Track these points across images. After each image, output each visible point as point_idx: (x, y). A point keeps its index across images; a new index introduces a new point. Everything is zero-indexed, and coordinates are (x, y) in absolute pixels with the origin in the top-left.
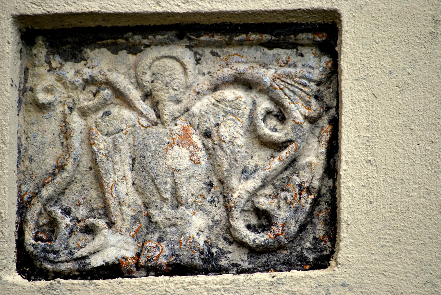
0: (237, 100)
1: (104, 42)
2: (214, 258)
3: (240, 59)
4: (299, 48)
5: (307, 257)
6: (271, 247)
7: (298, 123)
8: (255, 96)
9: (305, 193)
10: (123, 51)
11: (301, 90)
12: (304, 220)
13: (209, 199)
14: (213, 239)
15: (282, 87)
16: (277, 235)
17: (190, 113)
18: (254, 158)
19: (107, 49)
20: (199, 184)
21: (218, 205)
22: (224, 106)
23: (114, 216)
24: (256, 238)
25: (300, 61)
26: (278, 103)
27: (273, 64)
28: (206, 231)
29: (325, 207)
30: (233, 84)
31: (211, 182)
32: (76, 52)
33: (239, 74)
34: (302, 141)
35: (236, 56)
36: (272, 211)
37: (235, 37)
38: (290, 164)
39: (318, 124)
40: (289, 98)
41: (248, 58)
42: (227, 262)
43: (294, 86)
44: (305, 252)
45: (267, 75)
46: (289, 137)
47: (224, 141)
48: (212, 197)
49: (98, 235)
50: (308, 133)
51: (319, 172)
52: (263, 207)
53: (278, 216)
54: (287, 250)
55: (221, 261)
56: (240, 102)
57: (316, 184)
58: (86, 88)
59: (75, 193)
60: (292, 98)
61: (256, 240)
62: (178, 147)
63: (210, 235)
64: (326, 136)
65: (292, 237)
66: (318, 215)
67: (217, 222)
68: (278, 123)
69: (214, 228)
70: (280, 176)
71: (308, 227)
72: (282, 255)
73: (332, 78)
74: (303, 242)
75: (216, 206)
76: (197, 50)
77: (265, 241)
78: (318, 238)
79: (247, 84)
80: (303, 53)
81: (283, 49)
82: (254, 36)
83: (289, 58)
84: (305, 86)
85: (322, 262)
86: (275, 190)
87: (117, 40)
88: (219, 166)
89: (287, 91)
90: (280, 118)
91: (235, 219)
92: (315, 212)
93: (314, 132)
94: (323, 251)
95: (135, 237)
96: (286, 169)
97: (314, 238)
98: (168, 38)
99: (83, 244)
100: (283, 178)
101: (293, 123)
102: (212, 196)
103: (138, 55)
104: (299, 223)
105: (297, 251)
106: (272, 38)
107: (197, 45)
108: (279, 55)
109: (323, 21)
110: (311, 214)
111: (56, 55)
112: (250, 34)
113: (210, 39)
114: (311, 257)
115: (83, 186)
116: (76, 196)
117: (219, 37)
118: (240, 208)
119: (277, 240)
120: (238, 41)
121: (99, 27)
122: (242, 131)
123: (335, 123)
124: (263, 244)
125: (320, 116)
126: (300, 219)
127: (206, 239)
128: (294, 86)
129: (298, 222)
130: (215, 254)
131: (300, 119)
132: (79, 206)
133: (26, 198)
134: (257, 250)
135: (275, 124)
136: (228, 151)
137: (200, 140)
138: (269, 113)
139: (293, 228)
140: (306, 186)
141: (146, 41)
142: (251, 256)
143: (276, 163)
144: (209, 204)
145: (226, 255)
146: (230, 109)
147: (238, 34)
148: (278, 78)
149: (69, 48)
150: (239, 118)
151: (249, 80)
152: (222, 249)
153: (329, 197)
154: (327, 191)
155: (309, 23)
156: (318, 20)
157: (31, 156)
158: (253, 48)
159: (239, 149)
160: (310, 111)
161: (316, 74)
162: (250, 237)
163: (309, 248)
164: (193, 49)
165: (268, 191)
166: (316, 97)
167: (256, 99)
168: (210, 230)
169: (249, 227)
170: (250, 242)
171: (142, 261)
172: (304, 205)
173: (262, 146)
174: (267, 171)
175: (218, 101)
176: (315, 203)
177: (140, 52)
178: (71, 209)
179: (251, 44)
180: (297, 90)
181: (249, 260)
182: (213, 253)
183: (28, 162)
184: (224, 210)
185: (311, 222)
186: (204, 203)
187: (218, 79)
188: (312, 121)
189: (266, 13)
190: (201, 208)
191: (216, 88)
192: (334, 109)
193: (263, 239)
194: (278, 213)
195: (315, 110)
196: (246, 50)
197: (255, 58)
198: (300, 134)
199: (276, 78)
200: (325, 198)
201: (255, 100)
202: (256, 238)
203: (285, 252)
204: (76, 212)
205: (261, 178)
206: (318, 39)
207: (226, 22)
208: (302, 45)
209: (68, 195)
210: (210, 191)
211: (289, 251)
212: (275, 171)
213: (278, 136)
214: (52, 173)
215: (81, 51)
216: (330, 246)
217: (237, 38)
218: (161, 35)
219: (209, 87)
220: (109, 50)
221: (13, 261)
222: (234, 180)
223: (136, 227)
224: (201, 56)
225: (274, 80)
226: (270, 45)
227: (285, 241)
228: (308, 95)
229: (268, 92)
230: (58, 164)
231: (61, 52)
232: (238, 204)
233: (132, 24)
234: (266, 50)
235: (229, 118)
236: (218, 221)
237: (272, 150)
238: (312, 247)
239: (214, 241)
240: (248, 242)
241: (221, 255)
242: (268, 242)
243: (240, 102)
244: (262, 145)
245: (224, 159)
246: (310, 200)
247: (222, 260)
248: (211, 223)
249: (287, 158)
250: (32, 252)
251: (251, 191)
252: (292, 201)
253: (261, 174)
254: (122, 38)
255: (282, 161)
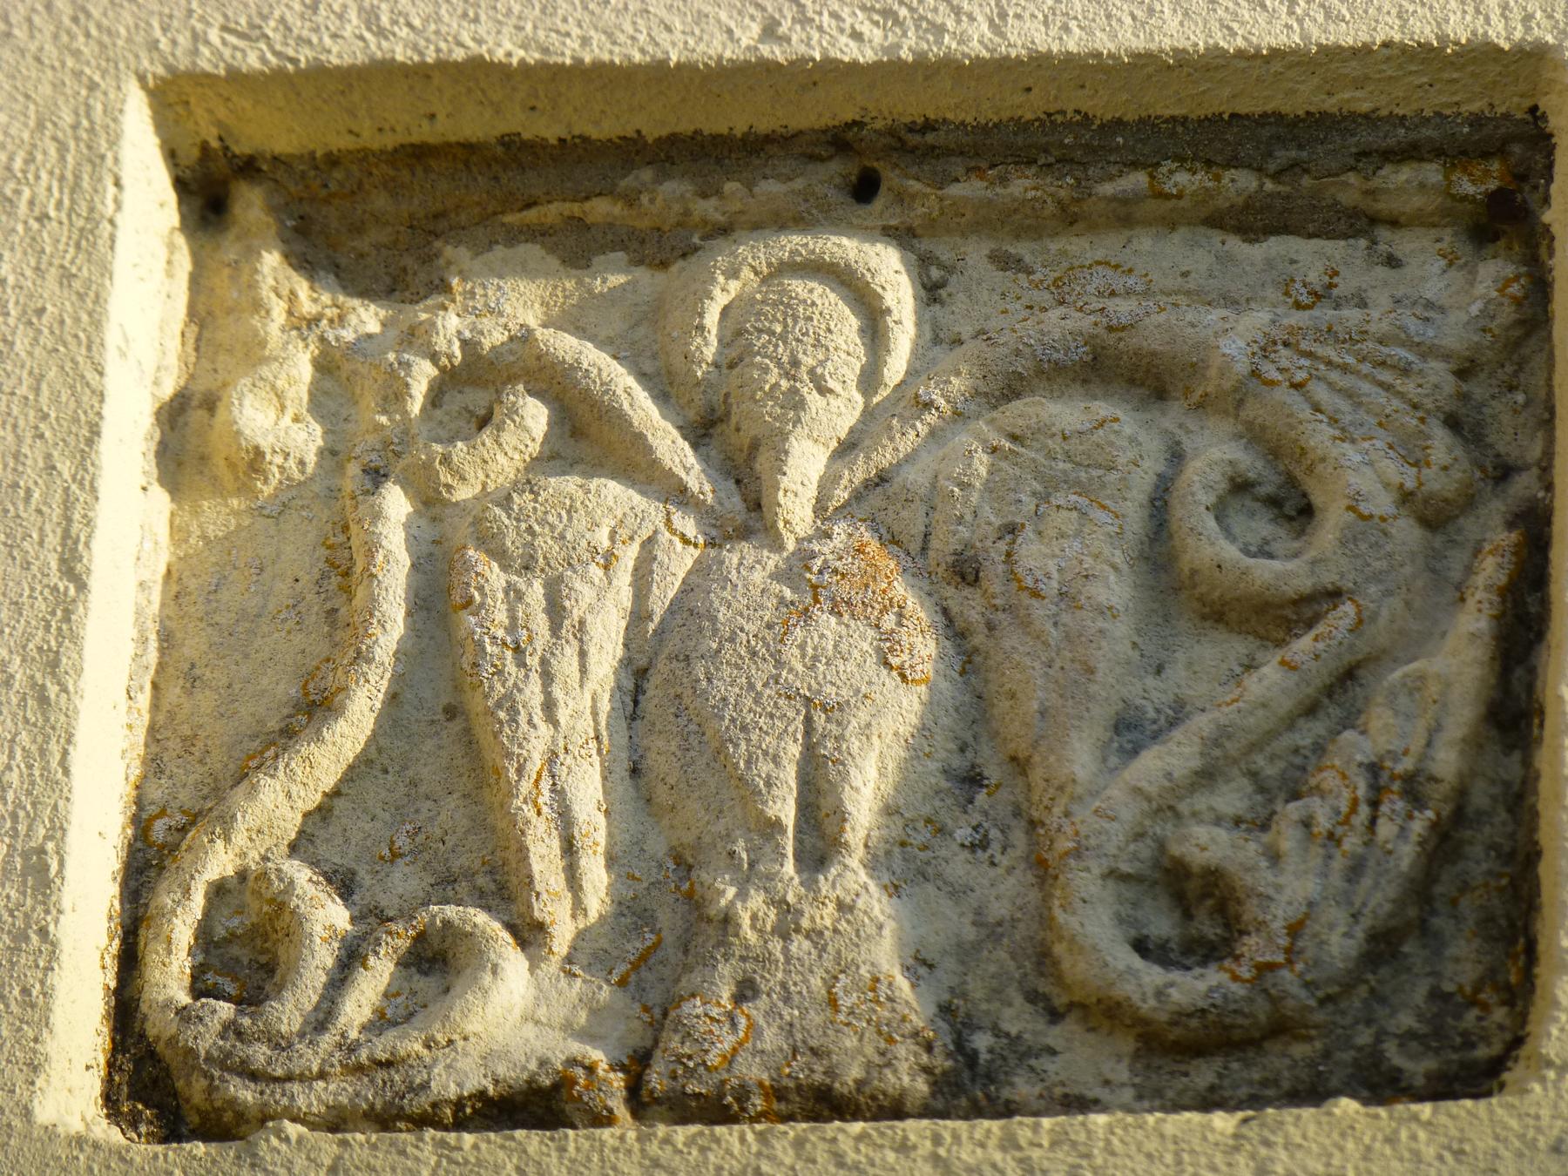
0: (1101, 432)
1: (531, 215)
2: (981, 1070)
3: (1118, 283)
4: (1383, 233)
5: (1399, 1070)
6: (1240, 1021)
7: (1371, 516)
8: (1180, 426)
9: (1395, 797)
10: (612, 255)
11: (1387, 387)
12: (1388, 907)
13: (963, 833)
14: (978, 995)
15: (1300, 376)
16: (1265, 968)
17: (891, 491)
18: (1168, 672)
19: (543, 245)
20: (920, 768)
21: (1004, 861)
22: (1040, 458)
23: (544, 896)
24: (1172, 985)
25: (1386, 283)
26: (1273, 446)
27: (1264, 299)
28: (950, 964)
29: (1484, 866)
30: (1085, 381)
31: (973, 767)
32: (409, 261)
33: (1110, 329)
34: (1388, 593)
35: (1100, 268)
36: (1248, 870)
37: (1102, 180)
38: (1329, 691)
39: (1459, 531)
40: (1333, 421)
41: (1154, 276)
42: (1037, 1090)
43: (1357, 373)
44: (1391, 1049)
45: (1233, 338)
46: (1328, 578)
47: (1036, 594)
48: (975, 829)
49: (469, 971)
50: (1413, 561)
51: (1462, 715)
52: (1207, 854)
53: (1271, 892)
54: (1309, 1039)
55: (1012, 1084)
56: (1112, 437)
57: (1447, 762)
58: (447, 397)
59: (379, 812)
60: (1347, 419)
61: (1172, 991)
62: (833, 620)
63: (965, 983)
64: (1491, 571)
65: (1330, 981)
66: (1454, 903)
67: (1000, 930)
68: (1282, 532)
69: (985, 953)
70: (1287, 740)
71: (1406, 949)
72: (1287, 1061)
73: (1526, 351)
74: (1381, 1012)
75: (993, 864)
76: (931, 247)
77: (1211, 990)
78: (1451, 995)
79: (1149, 379)
80: (1399, 254)
81: (1310, 236)
82: (1182, 178)
83: (1336, 273)
84: (1405, 371)
85: (1475, 1074)
86: (1259, 798)
87: (587, 205)
88: (1012, 696)
89: (1321, 393)
90: (1289, 509)
91: (1078, 904)
92: (1438, 889)
93: (1438, 566)
94: (1473, 1046)
95: (632, 988)
96: (1311, 710)
97: (1436, 995)
98: (806, 195)
99: (402, 1012)
100: (1296, 751)
101: (1351, 516)
102: (979, 825)
103: (674, 269)
104: (1366, 922)
105: (1352, 1047)
106: (1262, 186)
107: (933, 226)
108: (1293, 262)
109: (1492, 106)
110: (1421, 888)
111: (322, 273)
112: (1164, 170)
113: (989, 193)
114: (1418, 1068)
115: (414, 784)
116: (379, 825)
117: (1028, 183)
118: (1104, 860)
119: (1265, 991)
120: (1114, 199)
121: (510, 143)
122: (1118, 552)
123: (1534, 531)
124: (1201, 1004)
125: (1469, 501)
126: (1372, 903)
127: (946, 997)
128: (1357, 373)
129: (1362, 919)
130: (984, 1057)
131: (1382, 504)
132: (392, 862)
133: (159, 831)
134: (1175, 1034)
135: (1264, 533)
136: (1054, 634)
137: (930, 595)
138: (1240, 486)
139: (1339, 944)
140: (1400, 768)
141: (708, 209)
142: (1148, 1067)
143: (1273, 679)
144: (966, 854)
145: (1033, 1062)
146: (1068, 466)
147: (1114, 170)
148: (1286, 344)
149: (377, 247)
150: (1108, 502)
151: (1154, 354)
152: (1019, 1037)
153: (1504, 824)
154: (1494, 798)
155: (1428, 113)
156: (1470, 100)
157: (193, 666)
158: (1176, 237)
159: (1100, 624)
160: (1425, 471)
161: (1454, 332)
162: (1148, 985)
163: (1411, 1035)
164: (915, 241)
165: (1232, 798)
166: (1453, 423)
167: (1184, 439)
168: (963, 963)
169: (1141, 946)
170: (1144, 1001)
171: (656, 1080)
172: (1390, 846)
173: (1208, 624)
174: (1226, 709)
175: (1014, 438)
176: (1444, 844)
177: (684, 256)
178: (354, 873)
179: (1172, 217)
180: (1366, 387)
181: (1137, 1080)
182: (975, 1052)
183: (178, 690)
184: (1030, 878)
185: (1423, 928)
186: (943, 853)
187: (1018, 353)
188: (1436, 517)
189: (1243, 64)
190: (930, 870)
191: (1011, 389)
192: (1535, 471)
193: (1202, 986)
194: (1271, 878)
195: (1445, 468)
196: (1144, 242)
197: (1185, 274)
198: (1377, 565)
199: (1275, 343)
200: (1487, 830)
201: (1178, 443)
202: (1172, 985)
203: (1300, 1050)
204: (378, 889)
205: (1196, 739)
206: (1468, 188)
207: (1063, 112)
208: (1394, 223)
209: (344, 820)
210: (971, 802)
211: (1318, 1045)
212: (1260, 713)
213: (1285, 571)
214: (281, 731)
215: (429, 259)
216: (1507, 1022)
217: (1107, 189)
218: (778, 177)
219: (980, 383)
220: (552, 250)
221: (88, 1068)
222: (1077, 745)
223: (638, 945)
224: (949, 269)
225: (1266, 349)
226: (1251, 222)
227: (1303, 993)
228: (1415, 407)
229: (1240, 403)
230: (306, 694)
231: (343, 261)
232: (1093, 842)
233: (653, 124)
234: (1235, 244)
235: (1061, 502)
236: (1000, 924)
237: (1251, 638)
238: (1422, 1029)
239: (984, 1006)
240: (1136, 998)
241: (1012, 1061)
242: (1225, 997)
243: (1112, 437)
244: (1204, 618)
245: (1037, 665)
246: (1418, 826)
247: (1016, 1080)
248: (970, 933)
249: (1317, 657)
250: (173, 1037)
251: (1153, 790)
252: (1339, 831)
253: (1202, 723)
254: (609, 192)
255: (1294, 668)
